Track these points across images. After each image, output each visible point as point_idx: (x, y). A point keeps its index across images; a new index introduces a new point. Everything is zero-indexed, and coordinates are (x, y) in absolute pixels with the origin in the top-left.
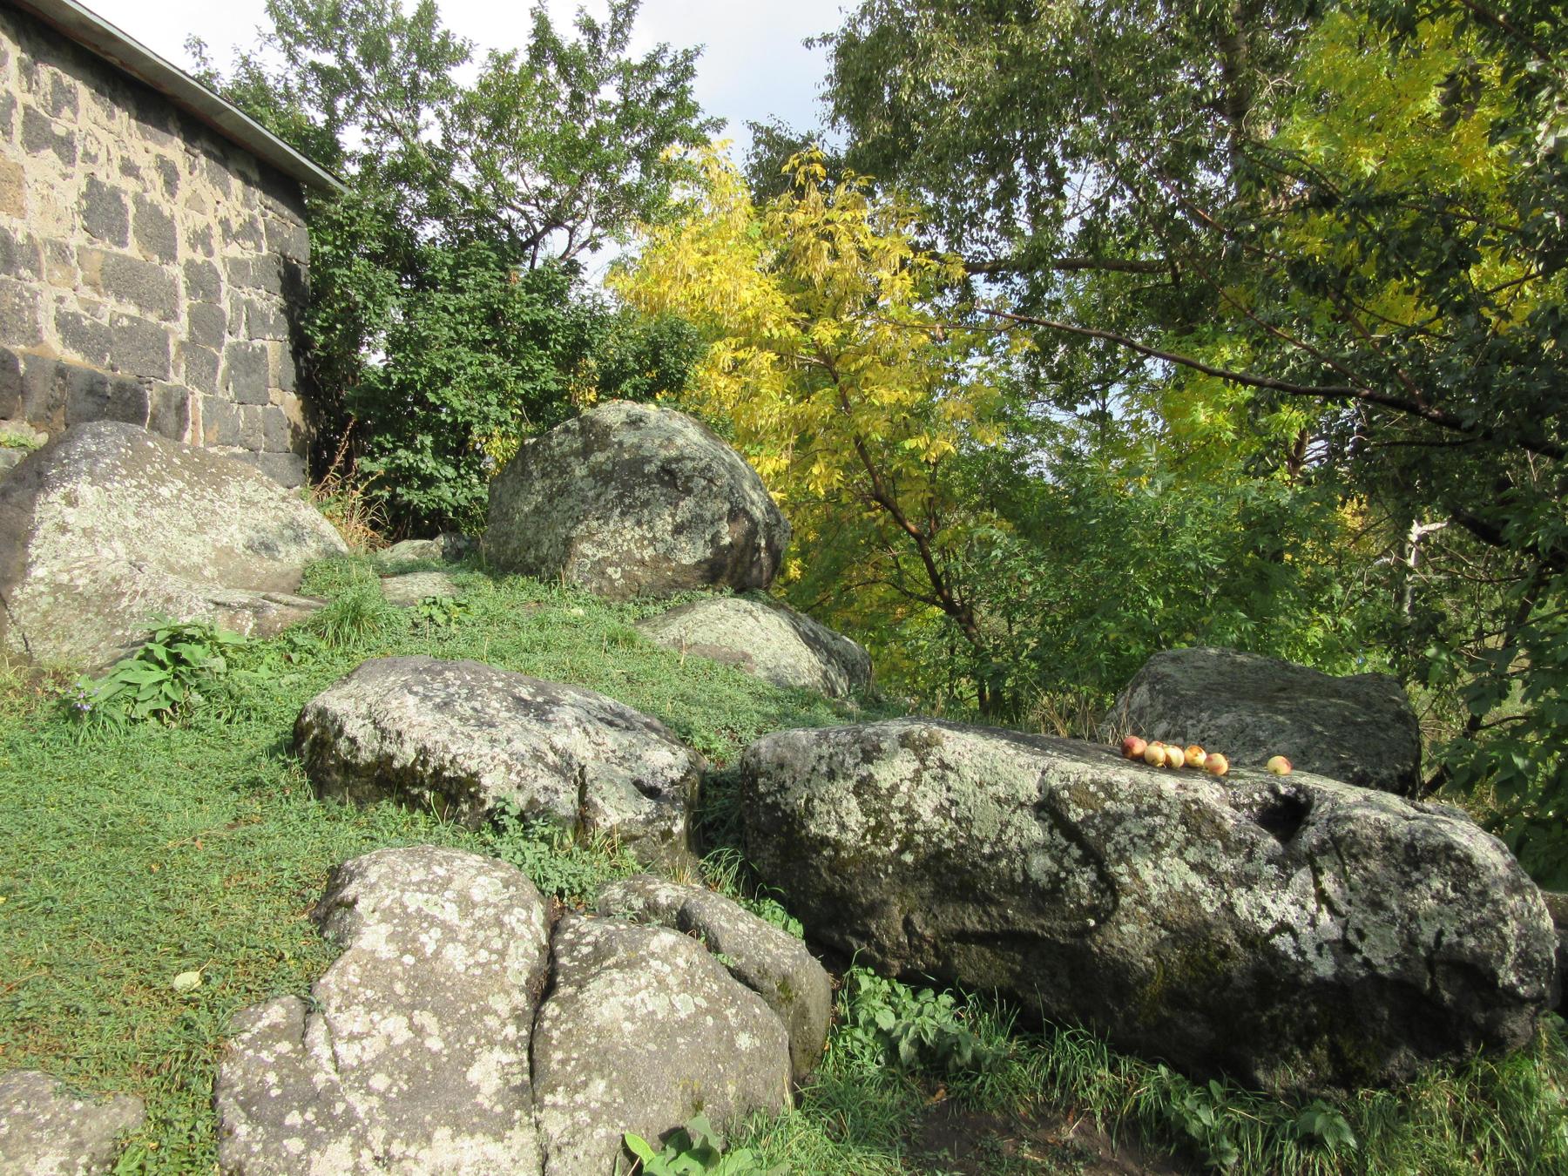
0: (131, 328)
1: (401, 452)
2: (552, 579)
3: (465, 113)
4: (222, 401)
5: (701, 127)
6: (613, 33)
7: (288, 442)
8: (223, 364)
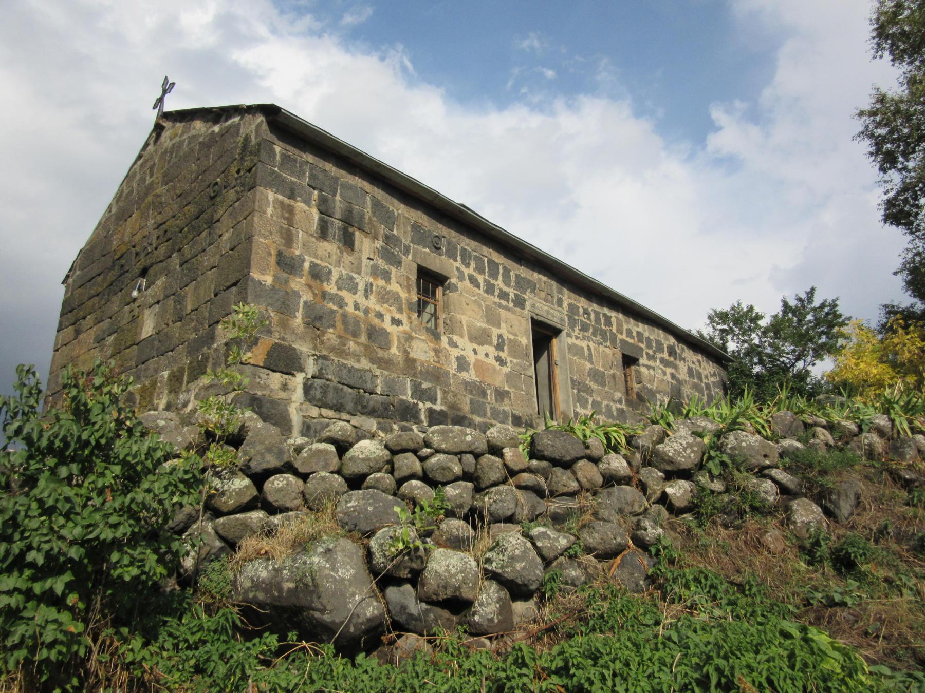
3: (765, 333)
5: (843, 321)
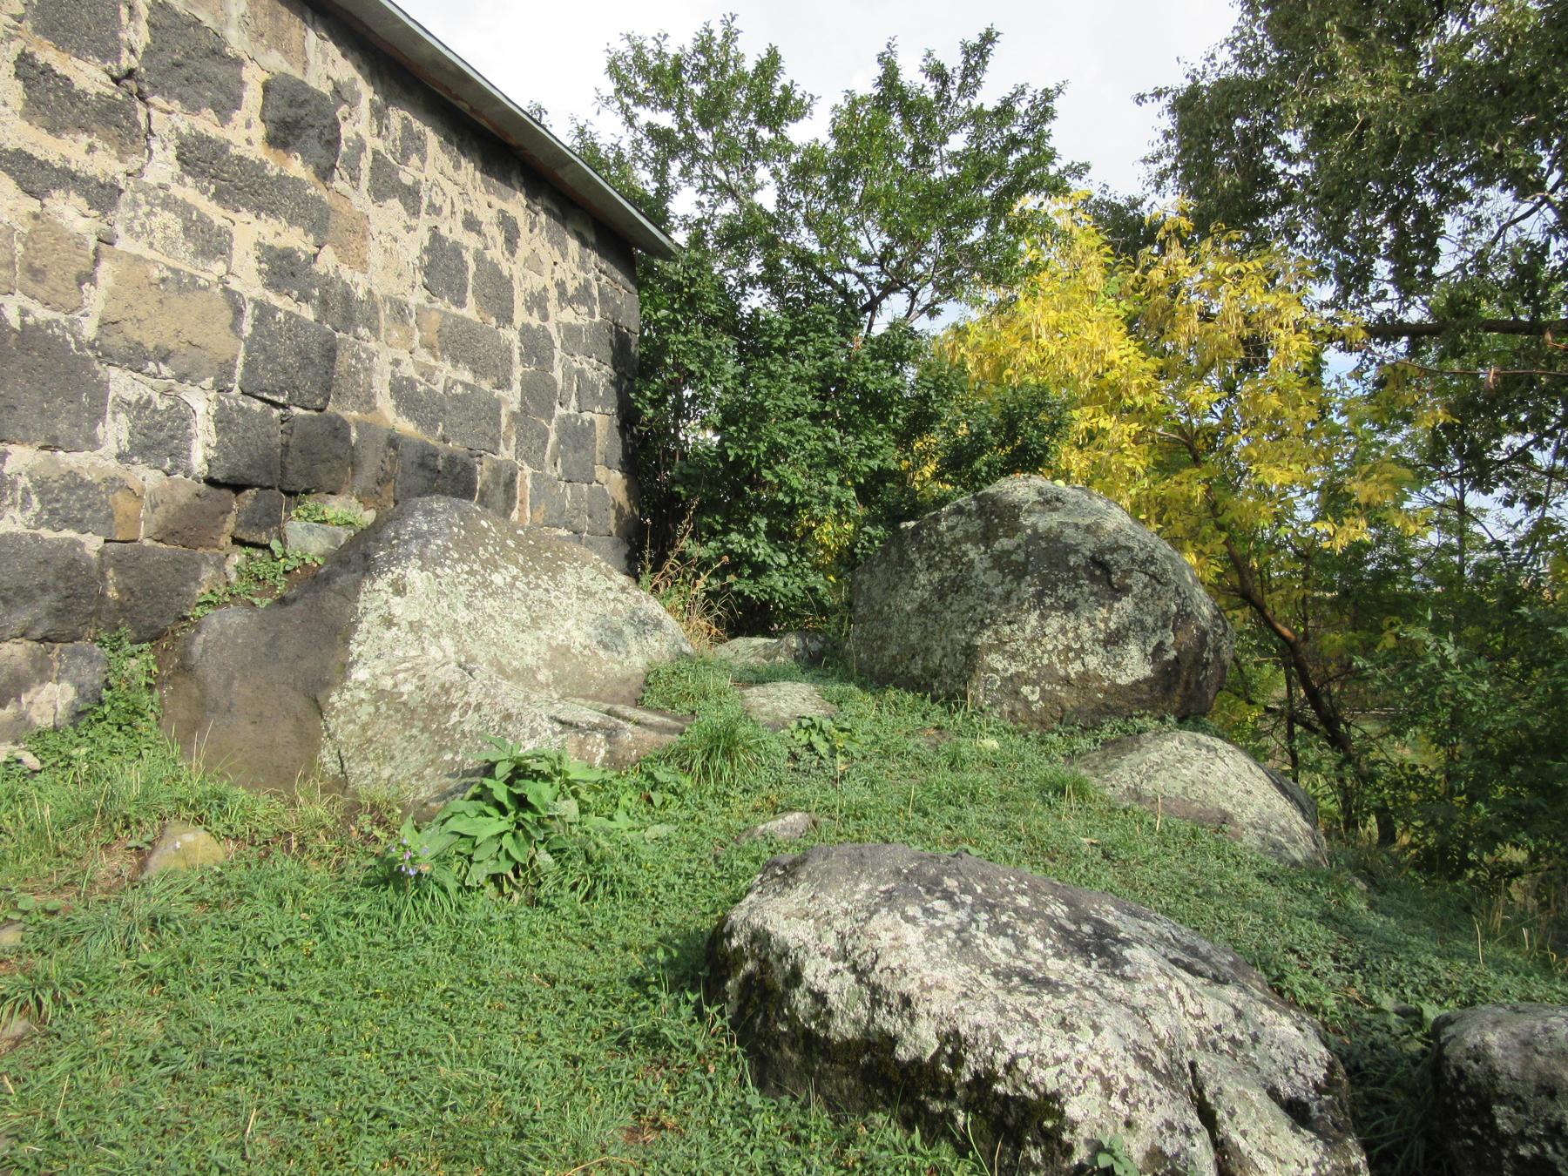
0: (464, 396)
1: (734, 536)
2: (953, 699)
3: (802, 172)
4: (549, 479)
6: (964, 77)
7: (612, 527)
8: (553, 438)
